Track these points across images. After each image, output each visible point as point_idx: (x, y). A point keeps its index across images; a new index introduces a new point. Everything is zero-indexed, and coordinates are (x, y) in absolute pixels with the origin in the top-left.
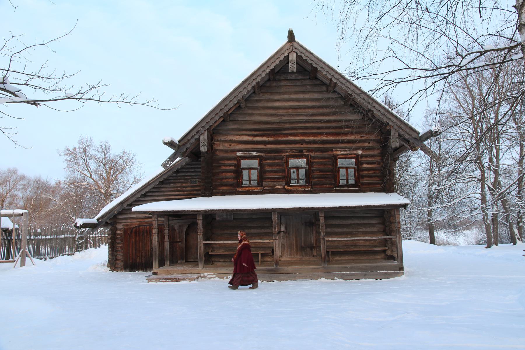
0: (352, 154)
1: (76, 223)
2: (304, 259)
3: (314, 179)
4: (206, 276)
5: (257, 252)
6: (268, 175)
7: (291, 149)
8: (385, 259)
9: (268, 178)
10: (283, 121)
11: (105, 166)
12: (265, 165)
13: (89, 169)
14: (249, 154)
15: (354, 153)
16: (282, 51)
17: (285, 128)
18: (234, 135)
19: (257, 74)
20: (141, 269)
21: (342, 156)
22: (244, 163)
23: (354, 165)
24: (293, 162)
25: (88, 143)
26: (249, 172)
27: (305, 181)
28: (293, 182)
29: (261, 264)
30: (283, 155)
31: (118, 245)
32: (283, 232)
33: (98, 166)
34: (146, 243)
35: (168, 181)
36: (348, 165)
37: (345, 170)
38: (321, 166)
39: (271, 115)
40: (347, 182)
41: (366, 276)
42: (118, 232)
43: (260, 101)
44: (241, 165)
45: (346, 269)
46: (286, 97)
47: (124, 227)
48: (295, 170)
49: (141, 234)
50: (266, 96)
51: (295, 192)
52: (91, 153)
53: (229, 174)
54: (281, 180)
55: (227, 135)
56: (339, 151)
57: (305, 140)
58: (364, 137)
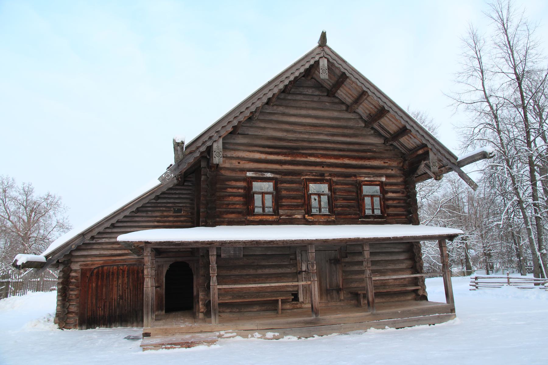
0: (376, 181)
1: (16, 261)
2: (330, 304)
3: (337, 208)
4: (223, 335)
5: (276, 299)
6: (285, 202)
7: (311, 172)
8: (416, 299)
9: (284, 205)
10: (301, 139)
11: (26, 208)
12: (281, 189)
13: (8, 211)
14: (262, 174)
15: (377, 180)
16: (312, 55)
17: (304, 147)
18: (244, 151)
19: (284, 77)
20: (104, 325)
21: (366, 183)
22: (257, 186)
23: (379, 193)
24: (313, 187)
25: (9, 184)
26: (262, 196)
27: (328, 209)
28: (314, 211)
29: (281, 314)
30: (302, 178)
31: (72, 293)
32: (305, 271)
33: (18, 208)
34: (112, 289)
35: (144, 209)
36: (373, 193)
37: (370, 198)
38: (345, 193)
39: (287, 131)
40: (373, 212)
41: (419, 322)
42: (73, 274)
43: (274, 114)
44: (252, 188)
45: (396, 314)
46: (303, 112)
47: (82, 267)
48: (316, 197)
49: (105, 277)
50: (281, 109)
51: (317, 223)
52: (11, 194)
53: (237, 199)
54: (300, 208)
55: (235, 151)
56: (363, 176)
57: (325, 162)
58: (387, 163)
